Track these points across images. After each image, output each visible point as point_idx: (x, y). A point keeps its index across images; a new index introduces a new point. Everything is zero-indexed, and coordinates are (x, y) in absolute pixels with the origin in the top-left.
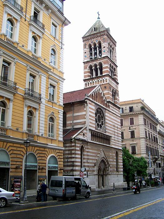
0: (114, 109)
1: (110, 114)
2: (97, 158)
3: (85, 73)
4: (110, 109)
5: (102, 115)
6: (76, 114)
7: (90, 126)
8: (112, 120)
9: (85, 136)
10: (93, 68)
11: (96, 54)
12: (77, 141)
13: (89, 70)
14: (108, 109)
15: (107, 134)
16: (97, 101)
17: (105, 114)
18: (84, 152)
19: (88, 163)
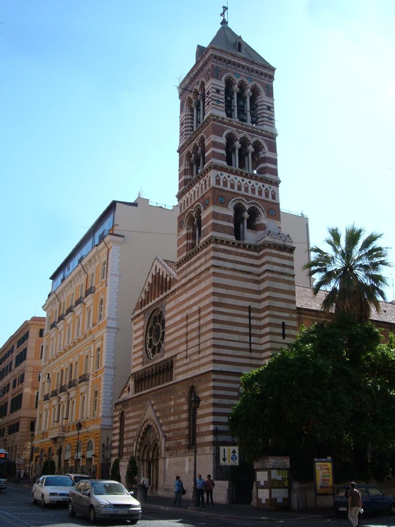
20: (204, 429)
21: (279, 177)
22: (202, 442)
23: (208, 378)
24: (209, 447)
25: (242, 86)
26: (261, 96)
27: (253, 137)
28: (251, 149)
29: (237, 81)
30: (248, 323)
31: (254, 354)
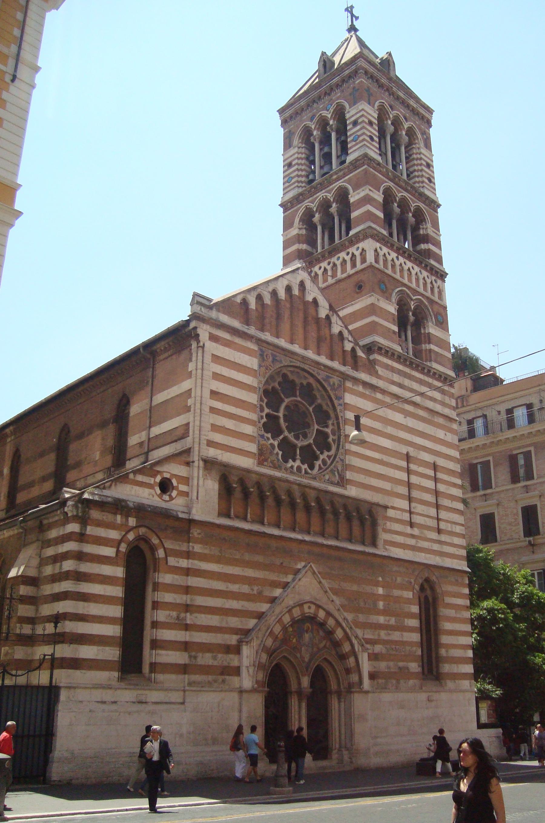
0: (407, 382)
1: (407, 414)
2: (264, 607)
3: (286, 244)
4: (379, 377)
5: (319, 401)
6: (160, 398)
7: (211, 444)
8: (390, 430)
9: (174, 493)
10: (317, 218)
11: (327, 157)
12: (95, 514)
13: (304, 232)
14: (363, 376)
15: (352, 492)
16: (312, 343)
17: (339, 398)
18: (155, 571)
19: (187, 627)
20: (457, 653)
21: (444, 267)
22: (455, 672)
23: (460, 580)
24: (468, 681)
25: (396, 123)
26: (417, 145)
27: (399, 192)
28: (396, 209)
29: (406, 125)
30: (407, 480)
31: (443, 538)
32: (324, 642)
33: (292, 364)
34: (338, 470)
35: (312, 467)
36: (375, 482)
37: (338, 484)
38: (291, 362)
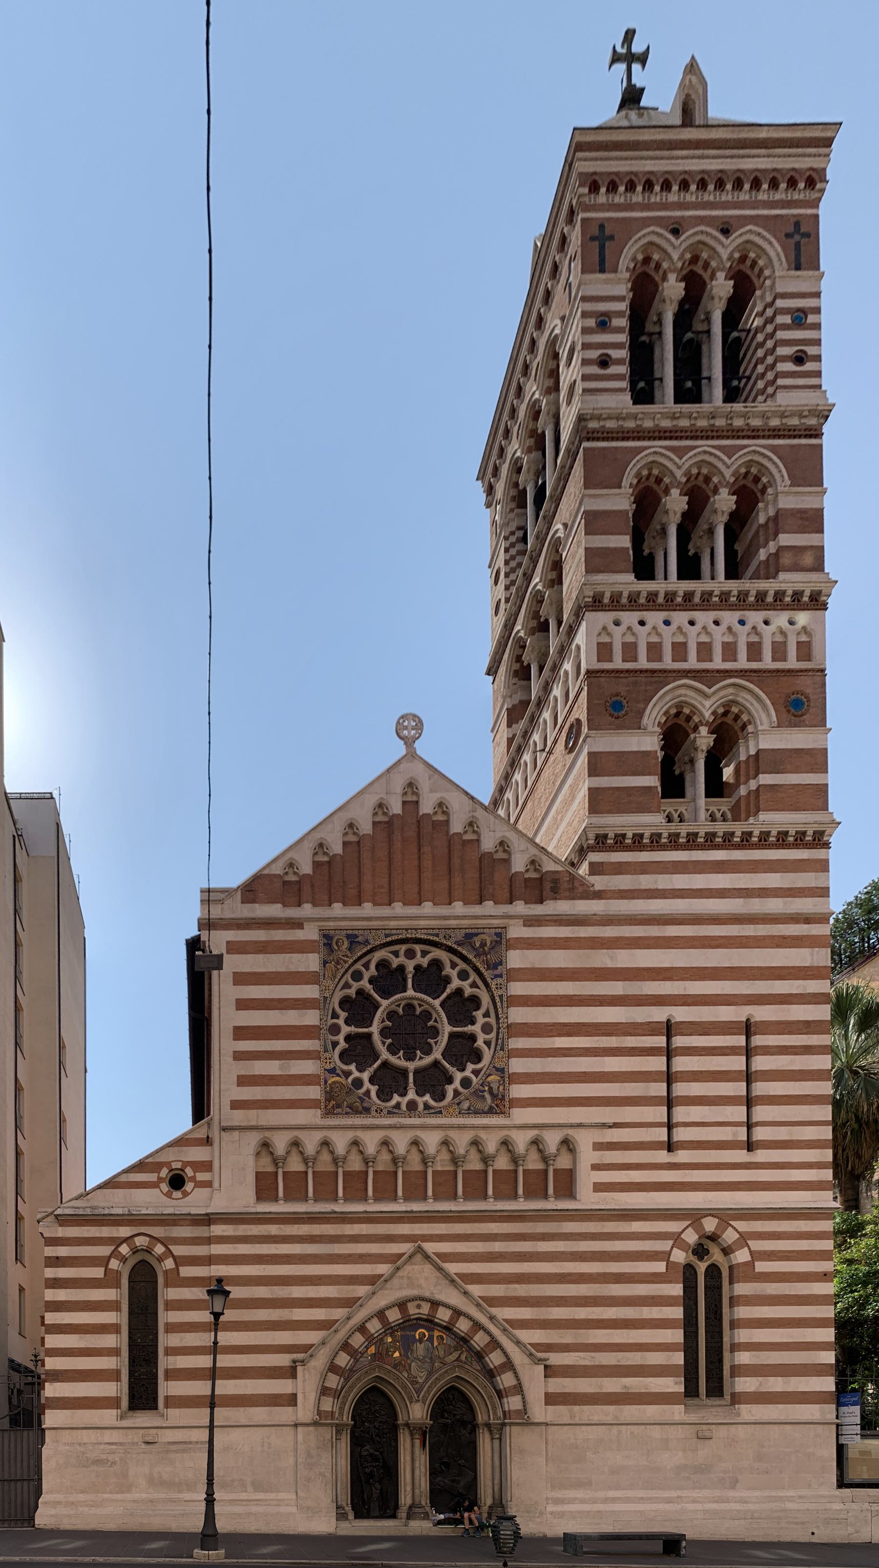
9: (189, 1186)
32: (455, 1355)
33: (389, 939)
34: (491, 1089)
35: (441, 1097)
36: (297, 1292)
37: (491, 1111)
38: (387, 936)
